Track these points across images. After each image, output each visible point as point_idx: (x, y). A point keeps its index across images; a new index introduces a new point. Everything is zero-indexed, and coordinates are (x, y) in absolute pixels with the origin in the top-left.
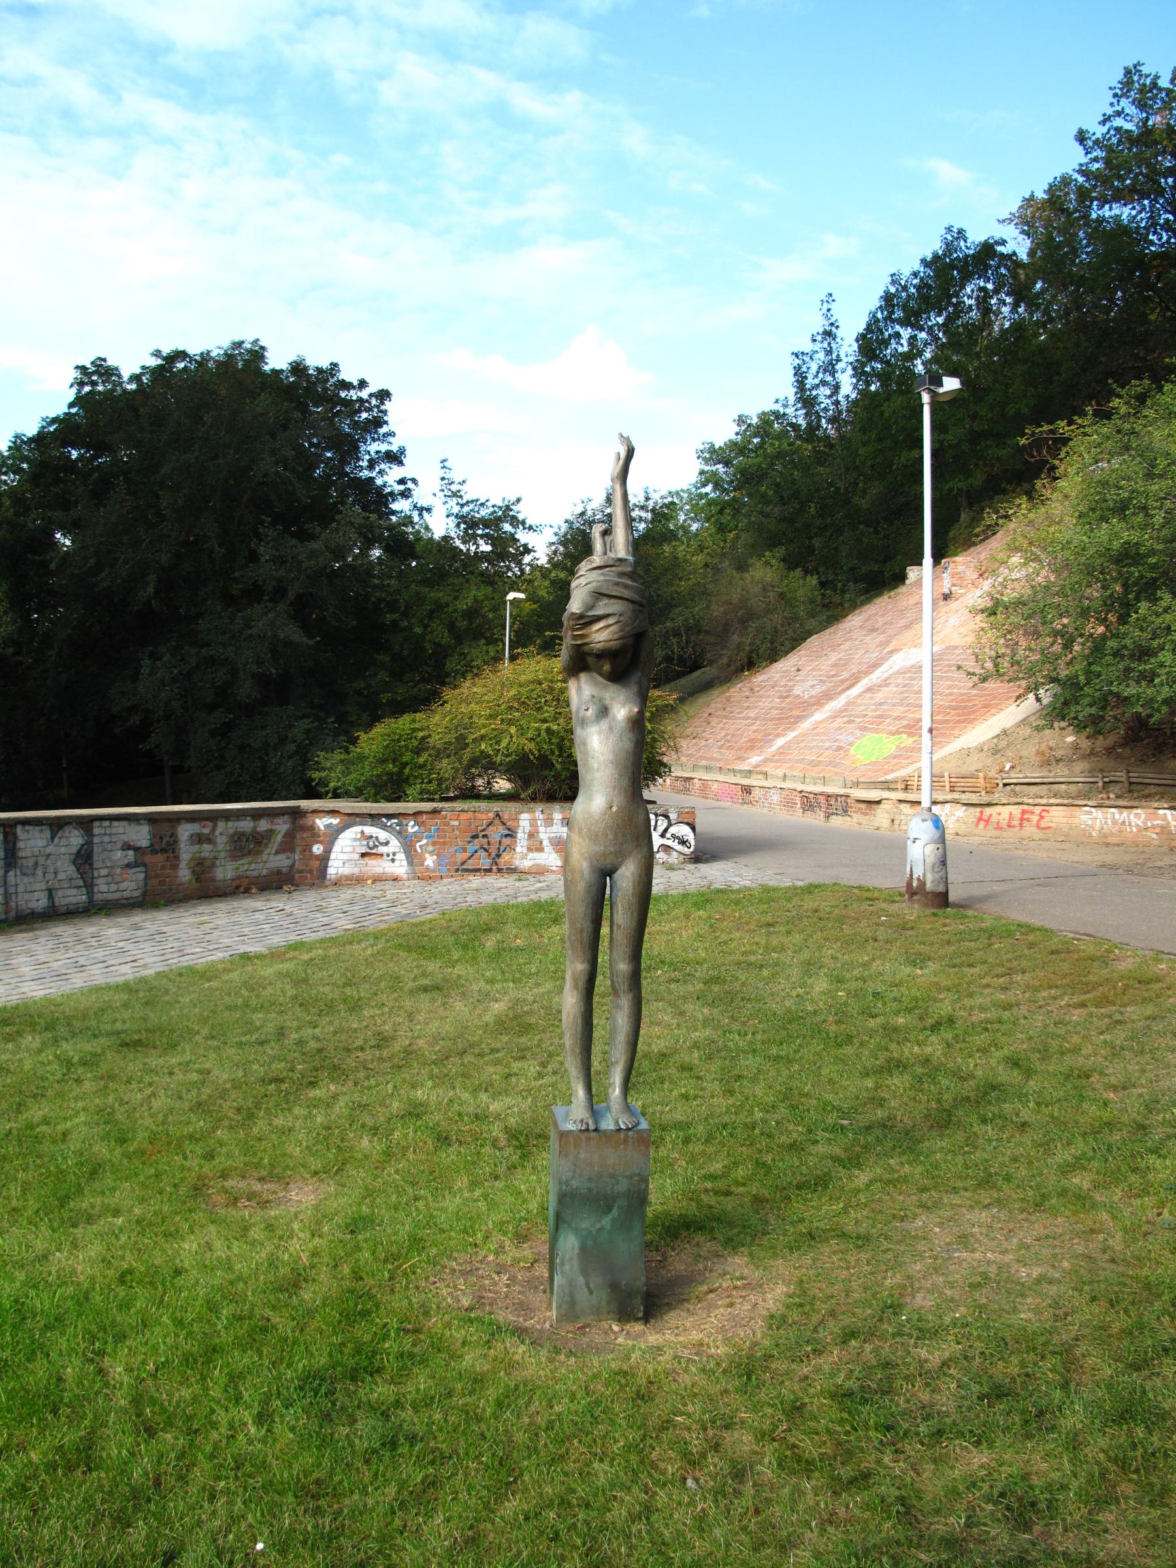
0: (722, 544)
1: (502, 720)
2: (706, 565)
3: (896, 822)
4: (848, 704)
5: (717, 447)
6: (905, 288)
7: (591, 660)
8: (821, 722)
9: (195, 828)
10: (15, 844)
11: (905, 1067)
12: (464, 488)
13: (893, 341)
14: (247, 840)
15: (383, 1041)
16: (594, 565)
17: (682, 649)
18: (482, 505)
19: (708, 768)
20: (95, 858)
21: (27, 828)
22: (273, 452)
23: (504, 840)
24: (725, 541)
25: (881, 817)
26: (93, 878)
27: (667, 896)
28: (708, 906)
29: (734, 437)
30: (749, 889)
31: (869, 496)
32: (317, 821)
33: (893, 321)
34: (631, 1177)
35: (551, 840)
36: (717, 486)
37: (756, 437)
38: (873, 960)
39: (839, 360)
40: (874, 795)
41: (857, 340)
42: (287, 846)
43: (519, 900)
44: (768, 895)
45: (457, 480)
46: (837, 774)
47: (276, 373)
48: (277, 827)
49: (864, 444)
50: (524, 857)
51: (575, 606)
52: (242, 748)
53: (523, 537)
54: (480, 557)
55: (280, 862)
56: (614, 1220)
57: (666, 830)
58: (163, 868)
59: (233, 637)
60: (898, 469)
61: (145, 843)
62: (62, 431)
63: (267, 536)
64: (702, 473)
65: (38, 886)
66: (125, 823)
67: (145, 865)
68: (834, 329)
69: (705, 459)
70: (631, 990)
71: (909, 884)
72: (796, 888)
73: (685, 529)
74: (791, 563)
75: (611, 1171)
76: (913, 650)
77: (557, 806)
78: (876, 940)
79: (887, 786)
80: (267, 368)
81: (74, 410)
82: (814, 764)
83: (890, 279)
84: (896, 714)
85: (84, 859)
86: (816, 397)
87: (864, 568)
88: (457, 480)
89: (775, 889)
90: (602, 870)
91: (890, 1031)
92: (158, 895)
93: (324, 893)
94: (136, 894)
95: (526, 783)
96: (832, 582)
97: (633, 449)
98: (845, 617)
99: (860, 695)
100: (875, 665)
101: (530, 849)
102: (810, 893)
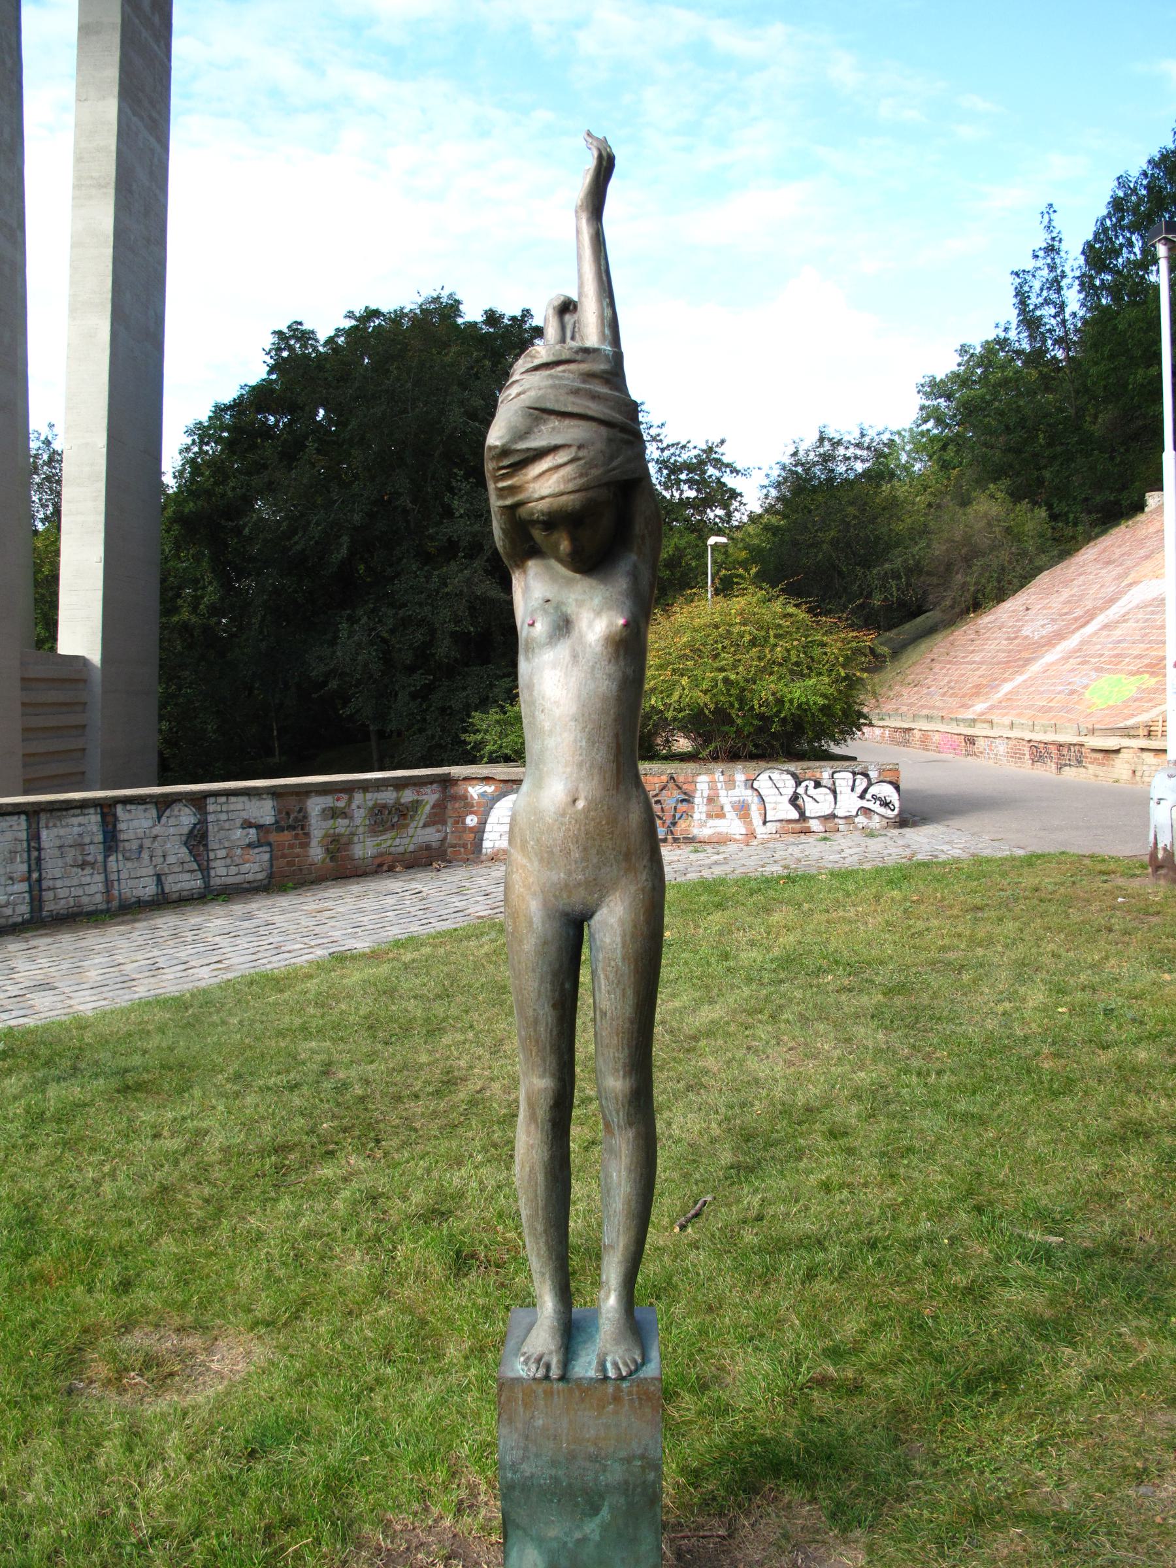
0: (945, 482)
1: (674, 670)
2: (930, 505)
3: (1138, 774)
4: (1083, 643)
5: (938, 380)
6: (1134, 191)
7: (538, 534)
8: (1053, 664)
9: (328, 801)
10: (115, 826)
11: (1147, 1135)
12: (663, 431)
13: (1125, 250)
14: (390, 813)
15: (450, 1082)
16: (537, 362)
17: (903, 593)
18: (684, 447)
19: (929, 718)
20: (211, 838)
21: (129, 807)
22: (462, 403)
23: (679, 805)
24: (949, 479)
25: (1121, 768)
26: (208, 860)
27: (857, 872)
28: (905, 885)
29: (955, 368)
30: (957, 860)
31: (1100, 422)
32: (470, 789)
33: (1123, 228)
34: (628, 1460)
35: (733, 805)
36: (939, 421)
37: (979, 366)
38: (1107, 958)
39: (1063, 275)
40: (1111, 743)
41: (1083, 253)
42: (438, 817)
43: (689, 876)
44: (980, 869)
45: (655, 424)
46: (1070, 720)
47: (473, 326)
48: (425, 797)
49: (1096, 364)
50: (703, 824)
51: (495, 436)
52: (443, 710)
53: (730, 481)
54: (685, 503)
55: (430, 835)
56: (605, 1528)
57: (865, 791)
58: (291, 847)
59: (429, 596)
60: (1134, 389)
61: (269, 819)
62: (258, 398)
63: (460, 490)
64: (922, 408)
65: (144, 872)
66: (245, 799)
67: (270, 844)
68: (1056, 243)
69: (925, 393)
70: (630, 1124)
71: (1153, 855)
72: (1014, 859)
73: (906, 468)
74: (1016, 496)
75: (592, 1449)
76: (1154, 581)
77: (739, 766)
78: (1110, 930)
79: (1127, 732)
80: (460, 321)
81: (274, 377)
82: (1045, 710)
83: (1116, 183)
84: (1135, 653)
85: (197, 840)
86: (1041, 317)
87: (1098, 498)
88: (655, 424)
89: (989, 861)
90: (567, 915)
91: (1126, 1072)
92: (286, 878)
93: (476, 870)
94: (260, 876)
95: (707, 739)
96: (1066, 514)
97: (614, 158)
98: (1078, 550)
99: (1096, 633)
100: (1112, 600)
101: (709, 816)
102: (1030, 865)
